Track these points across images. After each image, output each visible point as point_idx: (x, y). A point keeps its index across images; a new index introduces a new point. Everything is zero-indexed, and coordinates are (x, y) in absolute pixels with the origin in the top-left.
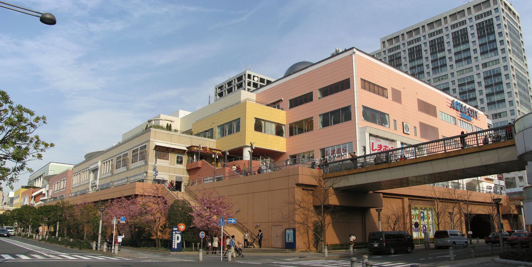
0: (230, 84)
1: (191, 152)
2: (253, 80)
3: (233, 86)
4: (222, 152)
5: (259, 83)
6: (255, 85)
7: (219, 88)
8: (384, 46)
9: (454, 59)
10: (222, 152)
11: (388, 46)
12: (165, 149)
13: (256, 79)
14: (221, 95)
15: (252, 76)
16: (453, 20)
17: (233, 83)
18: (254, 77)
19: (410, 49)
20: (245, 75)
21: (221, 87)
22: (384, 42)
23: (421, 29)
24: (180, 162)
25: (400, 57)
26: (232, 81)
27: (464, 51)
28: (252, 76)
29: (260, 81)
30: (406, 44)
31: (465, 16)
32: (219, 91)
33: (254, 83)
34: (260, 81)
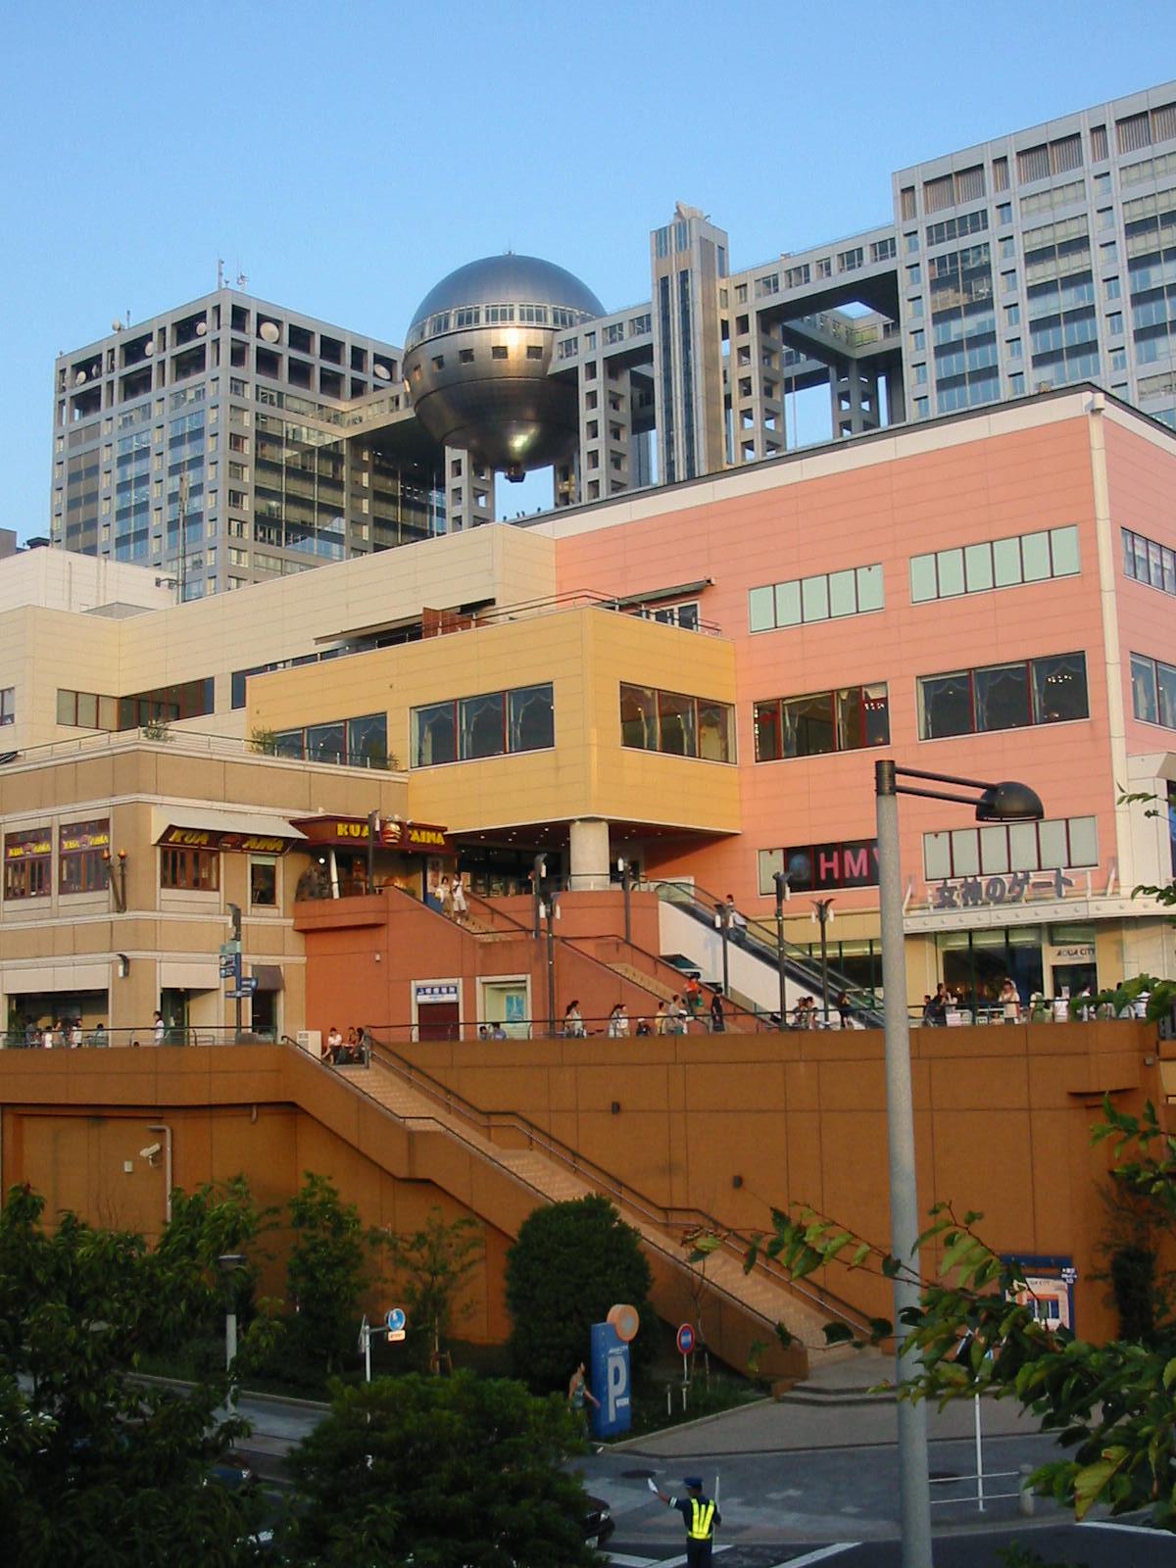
0: (134, 349)
1: (314, 841)
2: (258, 335)
3: (102, 381)
4: (447, 837)
5: (287, 353)
6: (267, 361)
8: (909, 212)
9: (1130, 321)
10: (447, 837)
11: (923, 220)
12: (743, 944)
14: (87, 402)
15: (253, 318)
16: (939, 205)
17: (150, 348)
18: (262, 319)
19: (942, 259)
20: (217, 309)
21: (88, 366)
22: (909, 190)
23: (1086, 141)
24: (264, 895)
25: (985, 270)
26: (149, 337)
27: (1074, 316)
28: (253, 318)
29: (292, 344)
30: (922, 235)
31: (1080, 163)
32: (81, 384)
34: (292, 344)
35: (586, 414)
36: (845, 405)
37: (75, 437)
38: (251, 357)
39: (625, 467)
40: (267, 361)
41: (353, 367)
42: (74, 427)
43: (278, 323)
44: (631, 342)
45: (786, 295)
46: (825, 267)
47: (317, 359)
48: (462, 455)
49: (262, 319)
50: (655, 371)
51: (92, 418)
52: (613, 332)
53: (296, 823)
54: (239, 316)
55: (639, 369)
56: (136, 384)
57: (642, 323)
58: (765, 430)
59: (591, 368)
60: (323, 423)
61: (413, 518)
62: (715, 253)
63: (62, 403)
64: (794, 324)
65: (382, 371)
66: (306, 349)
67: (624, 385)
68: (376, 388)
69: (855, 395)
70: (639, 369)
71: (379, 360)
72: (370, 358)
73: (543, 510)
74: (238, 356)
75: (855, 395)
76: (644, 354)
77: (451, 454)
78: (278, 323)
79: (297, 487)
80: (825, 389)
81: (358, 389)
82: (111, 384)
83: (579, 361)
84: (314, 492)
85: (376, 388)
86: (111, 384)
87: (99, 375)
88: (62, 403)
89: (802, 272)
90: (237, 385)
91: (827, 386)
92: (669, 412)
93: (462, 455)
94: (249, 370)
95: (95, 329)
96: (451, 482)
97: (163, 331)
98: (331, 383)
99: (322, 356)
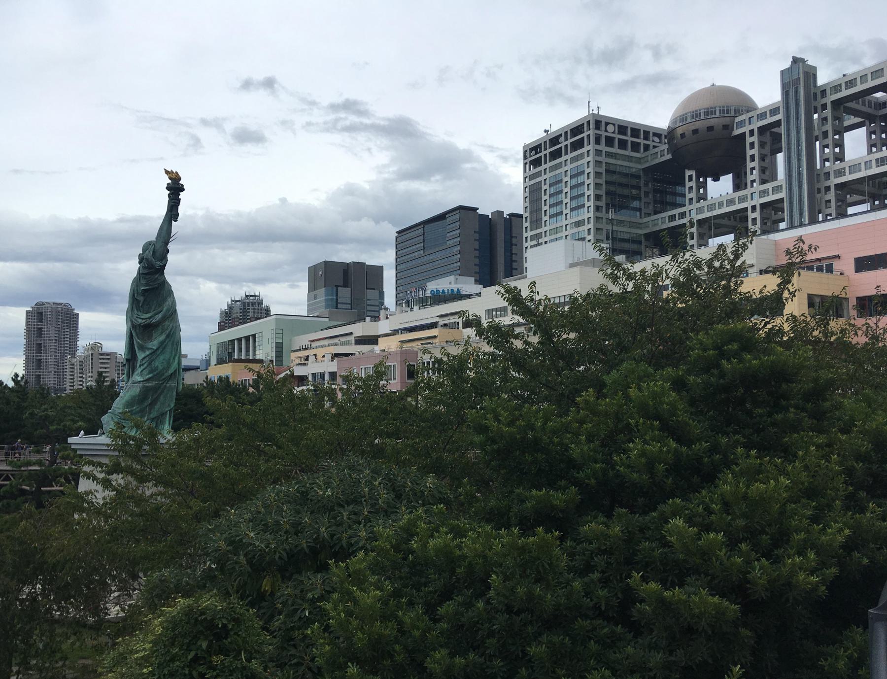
0: (555, 140)
2: (606, 131)
3: (542, 154)
5: (618, 136)
6: (609, 141)
7: (531, 150)
13: (610, 128)
14: (536, 163)
15: (603, 124)
17: (562, 139)
18: (607, 124)
21: (535, 148)
26: (561, 135)
28: (603, 124)
29: (619, 133)
33: (606, 137)
35: (749, 152)
36: (873, 136)
37: (532, 177)
38: (603, 140)
39: (767, 173)
40: (609, 141)
41: (877, 160)
42: (531, 173)
43: (614, 125)
44: (770, 120)
45: (845, 93)
46: (864, 78)
47: (630, 135)
48: (693, 173)
49: (607, 124)
50: (783, 130)
51: (538, 169)
52: (762, 116)
53: (298, 286)
54: (598, 124)
55: (775, 130)
56: (579, 144)
57: (774, 111)
58: (834, 153)
59: (752, 133)
60: (632, 162)
61: (669, 198)
62: (810, 74)
63: (526, 164)
64: (849, 105)
65: (657, 139)
66: (625, 134)
67: (767, 138)
68: (654, 147)
69: (878, 132)
70: (775, 130)
71: (655, 134)
72: (651, 134)
73: (882, 288)
74: (598, 141)
75: (878, 132)
76: (778, 123)
77: (688, 173)
78: (614, 125)
79: (626, 192)
80: (862, 131)
81: (647, 148)
82: (545, 155)
83: (746, 129)
84: (620, 191)
85: (654, 147)
86: (545, 163)
87: (541, 151)
88: (526, 164)
89: (850, 83)
90: (598, 152)
91: (865, 128)
92: (789, 144)
93: (693, 173)
94: (602, 147)
95: (535, 135)
96: (688, 184)
97: (566, 133)
98: (635, 147)
99: (632, 136)
